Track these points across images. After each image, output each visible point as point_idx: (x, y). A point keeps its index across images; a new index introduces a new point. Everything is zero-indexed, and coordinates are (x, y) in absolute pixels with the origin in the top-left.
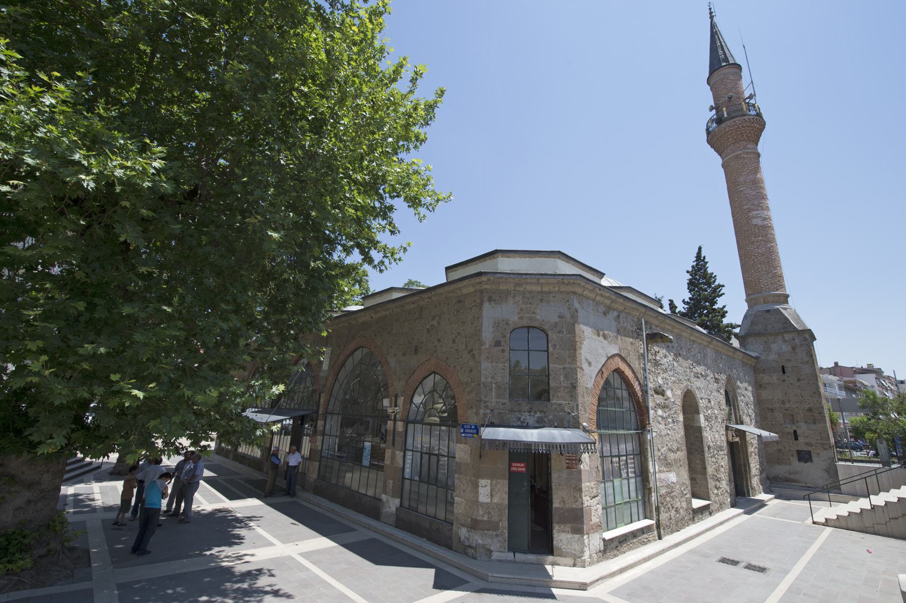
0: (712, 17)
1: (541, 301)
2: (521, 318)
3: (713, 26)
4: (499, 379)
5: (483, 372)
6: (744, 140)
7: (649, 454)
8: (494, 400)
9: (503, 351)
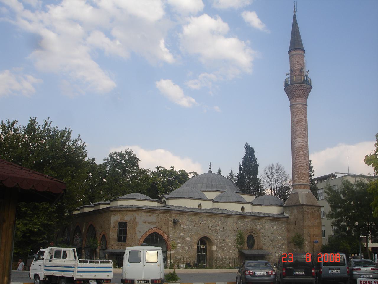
0: (294, 12)
1: (126, 214)
2: (121, 220)
3: (295, 17)
4: (114, 237)
5: (111, 235)
6: (296, 96)
7: (250, 261)
8: (113, 242)
9: (116, 229)
